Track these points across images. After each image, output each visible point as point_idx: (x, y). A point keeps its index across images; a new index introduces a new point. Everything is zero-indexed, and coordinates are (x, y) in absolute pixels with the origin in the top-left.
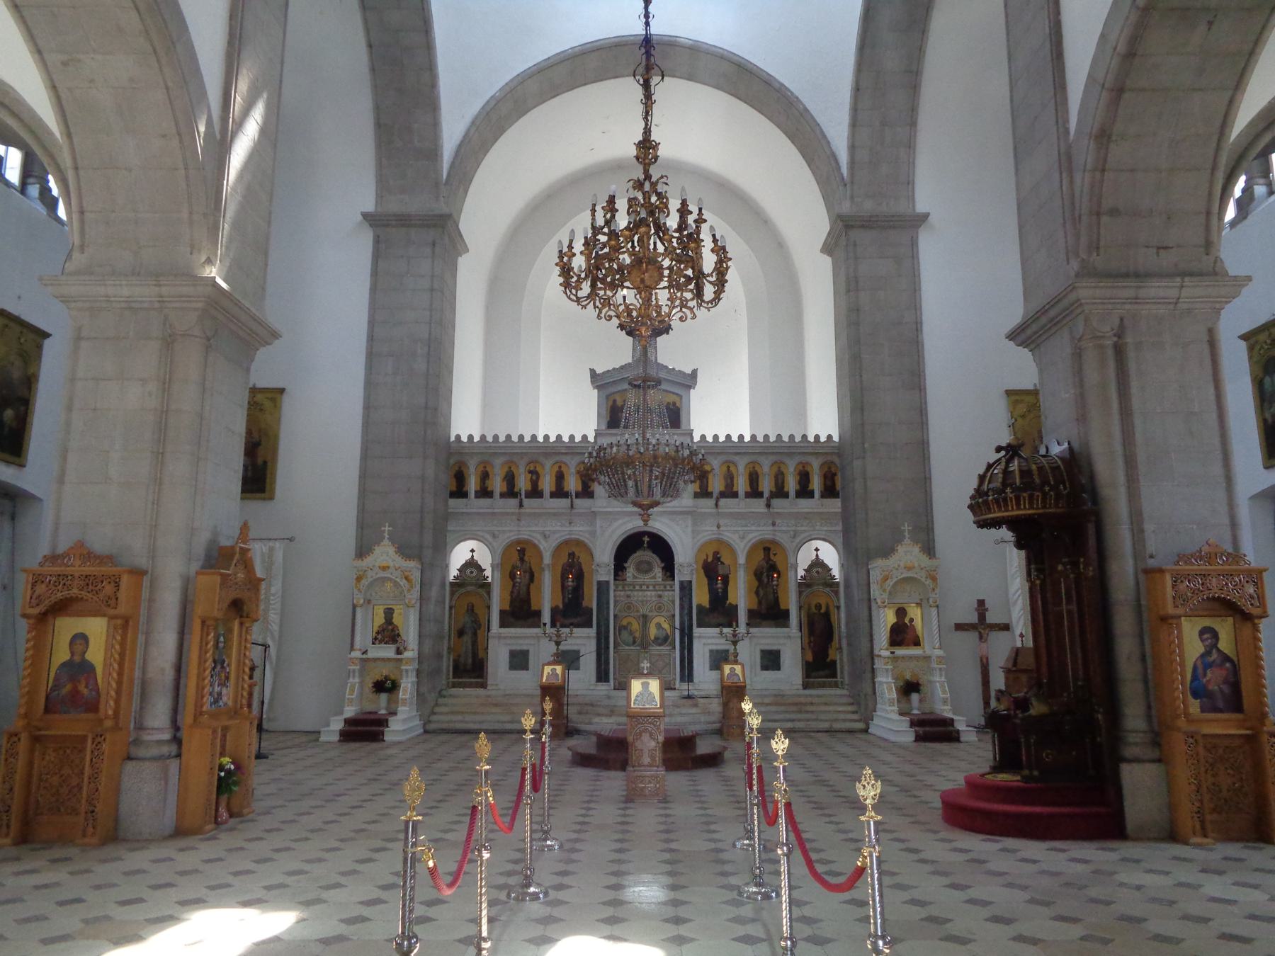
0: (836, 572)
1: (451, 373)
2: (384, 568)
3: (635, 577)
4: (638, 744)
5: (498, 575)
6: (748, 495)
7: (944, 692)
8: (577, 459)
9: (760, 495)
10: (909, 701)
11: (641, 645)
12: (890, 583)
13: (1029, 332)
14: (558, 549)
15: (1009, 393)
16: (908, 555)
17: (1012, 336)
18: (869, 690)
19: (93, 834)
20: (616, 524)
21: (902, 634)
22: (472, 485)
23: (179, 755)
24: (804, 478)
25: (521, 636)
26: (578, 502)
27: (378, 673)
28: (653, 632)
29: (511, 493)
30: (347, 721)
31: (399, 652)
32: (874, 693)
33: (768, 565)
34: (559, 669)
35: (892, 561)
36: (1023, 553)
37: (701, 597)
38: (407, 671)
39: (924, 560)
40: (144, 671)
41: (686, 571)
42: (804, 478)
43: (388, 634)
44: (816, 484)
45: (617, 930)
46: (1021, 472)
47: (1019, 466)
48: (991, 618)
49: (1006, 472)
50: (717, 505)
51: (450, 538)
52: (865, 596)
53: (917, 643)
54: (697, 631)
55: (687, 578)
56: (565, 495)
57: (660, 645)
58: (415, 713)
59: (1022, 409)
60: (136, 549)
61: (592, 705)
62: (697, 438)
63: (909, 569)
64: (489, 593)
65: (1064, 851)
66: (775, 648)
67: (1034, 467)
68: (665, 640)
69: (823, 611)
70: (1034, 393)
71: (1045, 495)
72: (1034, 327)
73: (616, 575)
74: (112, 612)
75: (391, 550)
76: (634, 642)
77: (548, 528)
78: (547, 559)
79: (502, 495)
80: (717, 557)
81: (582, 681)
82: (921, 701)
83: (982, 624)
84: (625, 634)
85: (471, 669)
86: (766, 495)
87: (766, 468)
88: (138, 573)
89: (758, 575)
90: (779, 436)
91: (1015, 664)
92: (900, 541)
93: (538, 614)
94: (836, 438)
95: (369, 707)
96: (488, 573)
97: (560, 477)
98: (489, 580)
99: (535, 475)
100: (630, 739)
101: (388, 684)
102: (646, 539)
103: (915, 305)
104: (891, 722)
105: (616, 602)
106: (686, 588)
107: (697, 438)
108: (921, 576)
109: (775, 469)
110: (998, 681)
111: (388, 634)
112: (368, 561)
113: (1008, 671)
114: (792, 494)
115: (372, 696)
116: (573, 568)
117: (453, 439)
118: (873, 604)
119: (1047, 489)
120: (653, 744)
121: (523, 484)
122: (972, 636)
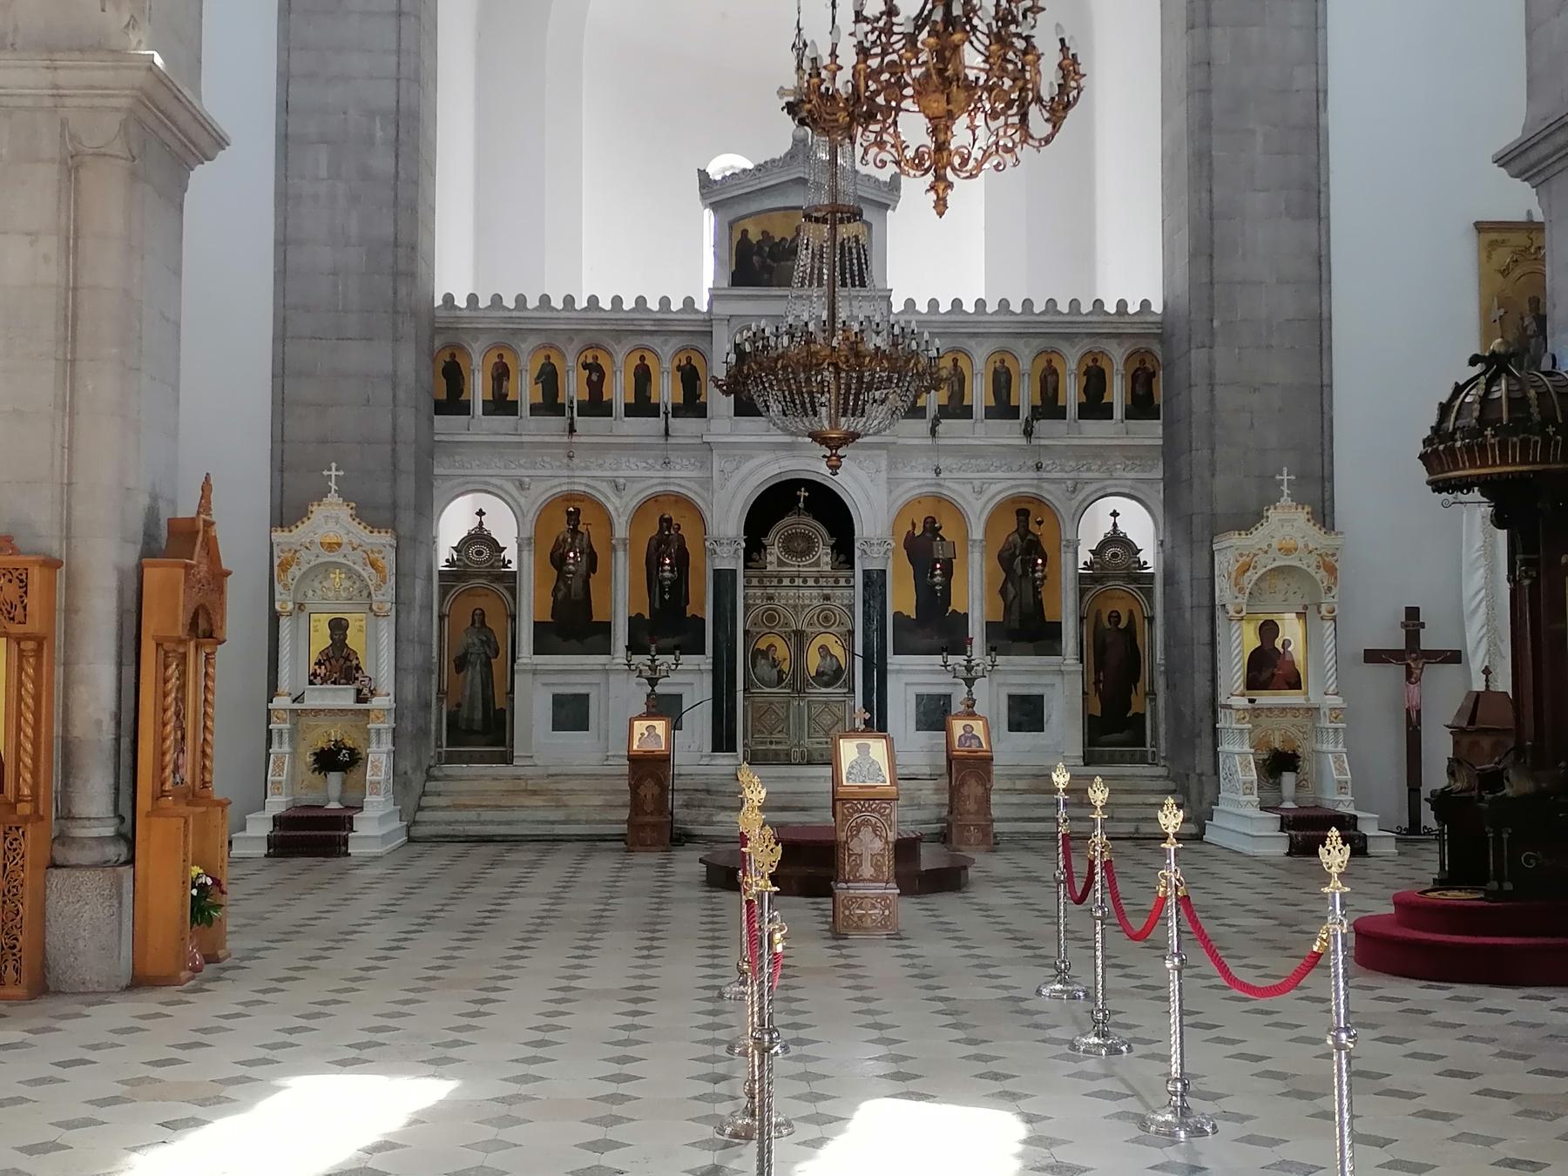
0: (1149, 556)
1: (433, 175)
2: (331, 547)
3: (781, 563)
4: (854, 845)
5: (529, 558)
6: (990, 413)
7: (1341, 771)
8: (675, 343)
9: (1013, 413)
10: (1278, 786)
11: (792, 686)
12: (1252, 576)
13: (1533, 156)
14: (641, 510)
15: (1481, 227)
16: (1287, 524)
17: (1504, 160)
18: (1209, 769)
19: (17, 982)
20: (747, 467)
21: (1268, 668)
22: (478, 388)
23: (131, 861)
24: (1095, 380)
25: (573, 670)
26: (675, 423)
27: (323, 735)
28: (814, 661)
29: (550, 405)
30: (278, 821)
31: (360, 698)
32: (1216, 773)
33: (1026, 543)
34: (660, 726)
35: (1257, 538)
36: (1502, 535)
37: (901, 598)
38: (378, 731)
39: (1315, 536)
40: (66, 723)
41: (876, 552)
42: (1095, 380)
43: (339, 664)
44: (1117, 393)
45: (912, 1085)
46: (1509, 399)
47: (1508, 391)
48: (1428, 642)
49: (1484, 400)
50: (933, 432)
51: (440, 487)
52: (1206, 601)
53: (1294, 683)
54: (894, 661)
55: (876, 566)
56: (653, 411)
57: (827, 685)
58: (392, 808)
59: (1503, 256)
60: (40, 524)
61: (708, 792)
62: (898, 307)
63: (1288, 551)
64: (513, 591)
65: (1548, 999)
66: (1035, 691)
67: (1532, 393)
68: (833, 676)
69: (1122, 625)
70: (1532, 227)
71: (1547, 440)
72: (1544, 149)
73: (748, 558)
74: (15, 629)
75: (345, 513)
76: (780, 680)
77: (624, 471)
78: (621, 531)
79: (535, 410)
80: (932, 527)
81: (691, 748)
82: (1298, 786)
83: (1412, 652)
84: (763, 667)
85: (482, 728)
86: (1025, 412)
87: (1025, 363)
88: (51, 564)
89: (1005, 559)
90: (1051, 302)
91: (1472, 721)
92: (1274, 502)
93: (606, 628)
94: (1157, 307)
95: (309, 798)
96: (510, 554)
97: (643, 376)
98: (513, 567)
99: (596, 374)
100: (842, 836)
101: (344, 756)
102: (803, 493)
103: (1315, 57)
104: (1245, 822)
105: (747, 607)
106: (875, 583)
107: (898, 307)
108: (1308, 564)
109: (1042, 363)
110: (1439, 748)
111: (339, 664)
112: (300, 533)
113: (1458, 732)
114: (1072, 411)
115: (317, 778)
116: (668, 544)
117: (438, 302)
118: (1219, 613)
119: (1551, 430)
120: (878, 845)
121: (573, 387)
122: (1392, 673)
